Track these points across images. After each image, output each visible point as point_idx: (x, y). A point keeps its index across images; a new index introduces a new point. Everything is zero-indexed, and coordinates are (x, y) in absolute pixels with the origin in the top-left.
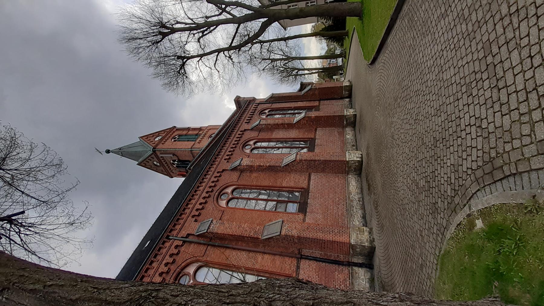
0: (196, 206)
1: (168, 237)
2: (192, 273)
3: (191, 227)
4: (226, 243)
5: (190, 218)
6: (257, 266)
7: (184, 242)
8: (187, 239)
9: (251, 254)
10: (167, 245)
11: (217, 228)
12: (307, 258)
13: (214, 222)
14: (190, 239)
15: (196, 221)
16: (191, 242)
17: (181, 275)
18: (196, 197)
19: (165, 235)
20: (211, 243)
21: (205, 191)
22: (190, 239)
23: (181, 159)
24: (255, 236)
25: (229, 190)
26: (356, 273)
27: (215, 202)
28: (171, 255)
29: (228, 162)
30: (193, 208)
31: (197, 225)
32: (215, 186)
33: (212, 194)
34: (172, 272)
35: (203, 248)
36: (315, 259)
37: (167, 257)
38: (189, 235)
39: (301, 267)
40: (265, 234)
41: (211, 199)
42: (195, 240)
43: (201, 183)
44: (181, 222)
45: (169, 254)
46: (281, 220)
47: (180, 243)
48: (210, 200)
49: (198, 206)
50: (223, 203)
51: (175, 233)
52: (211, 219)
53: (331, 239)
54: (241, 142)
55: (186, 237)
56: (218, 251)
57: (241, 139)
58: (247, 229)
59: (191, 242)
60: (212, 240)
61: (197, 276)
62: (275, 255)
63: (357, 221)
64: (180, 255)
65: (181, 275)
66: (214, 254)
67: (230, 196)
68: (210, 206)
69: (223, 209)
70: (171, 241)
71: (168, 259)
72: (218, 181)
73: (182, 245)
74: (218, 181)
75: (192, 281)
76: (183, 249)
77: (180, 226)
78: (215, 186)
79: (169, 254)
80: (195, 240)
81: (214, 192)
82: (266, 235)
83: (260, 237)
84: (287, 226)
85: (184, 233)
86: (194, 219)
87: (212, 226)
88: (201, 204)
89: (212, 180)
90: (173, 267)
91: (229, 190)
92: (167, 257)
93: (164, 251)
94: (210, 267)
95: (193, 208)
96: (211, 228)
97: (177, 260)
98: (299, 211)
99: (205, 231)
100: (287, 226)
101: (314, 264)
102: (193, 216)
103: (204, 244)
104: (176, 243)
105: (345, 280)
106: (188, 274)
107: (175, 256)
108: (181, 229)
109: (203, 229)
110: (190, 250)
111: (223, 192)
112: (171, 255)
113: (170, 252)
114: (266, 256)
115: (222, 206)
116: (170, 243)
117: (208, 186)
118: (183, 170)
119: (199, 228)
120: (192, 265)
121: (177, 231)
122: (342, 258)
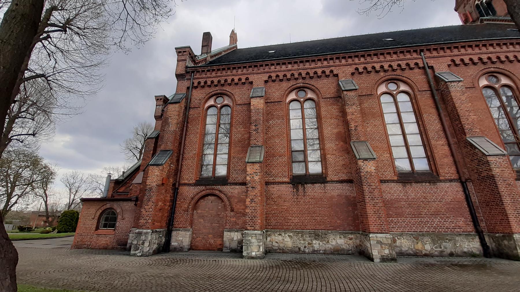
0: (466, 56)
1: (422, 51)
2: (400, 89)
3: (441, 66)
4: (441, 106)
5: (450, 58)
6: (433, 142)
7: (424, 68)
8: (428, 70)
9: (442, 132)
10: (415, 55)
11: (456, 91)
12: (465, 189)
13: (461, 84)
14: (429, 71)
15: (449, 66)
16: (426, 74)
17: (395, 81)
18: (477, 50)
19: (422, 48)
20: (435, 92)
21: (490, 55)
22: (429, 71)
23: (493, 3)
24: (466, 131)
25: (310, 95)
26: (473, 239)
27: (481, 73)
28: (408, 65)
29: (449, 66)
30: (381, 62)
31: (445, 69)
32: (502, 62)
33: (490, 65)
34: (395, 73)
35: (426, 87)
36: (468, 198)
37: (405, 62)
38: (432, 68)
39: (452, 183)
40: (356, 144)
41: (483, 67)
42: (431, 76)
43: (498, 45)
44: (442, 53)
45: (408, 61)
46: (375, 156)
47: (421, 65)
48: (481, 67)
49: (466, 60)
50: (483, 82)
51: (428, 54)
52: (462, 79)
53: (509, 212)
54: (308, 81)
55: (429, 67)
56: (430, 102)
57: (407, 71)
58: (470, 120)
59: (426, 74)
60: (439, 92)
61: (399, 94)
62: (453, 155)
63: (405, 244)
64: (411, 71)
65: (395, 81)
66: (426, 101)
67: (497, 86)
68: (472, 70)
69: (476, 85)
70: (419, 56)
71: (403, 64)
72: (511, 62)
73: (419, 68)
74: (511, 62)
75: (395, 92)
76: (416, 70)
77: (437, 55)
78: (502, 62)
79: (408, 61)
80: (431, 76)
81: (387, 74)
82: (476, 141)
83: (468, 136)
84: (501, 160)
85: (431, 62)
86: (450, 63)
87: (456, 84)
88: (471, 59)
89: (508, 54)
90: (399, 72)
91: (504, 81)
92: (405, 62)
93: (408, 56)
94: (316, 108)
95: (381, 62)
96: (453, 84)
97: (405, 71)
98: (517, 172)
99: (447, 81)
100: (501, 160)
101: (461, 195)
102: (453, 61)
103: (430, 86)
104: (420, 62)
105: (460, 227)
106: (398, 87)
107: (408, 68)
108: (434, 57)
109: (448, 77)
110: (417, 77)
111: (305, 89)
112: (408, 65)
113: (410, 62)
114: (446, 148)
115: (480, 82)
116: (418, 56)
117: (498, 54)
118: (475, 15)
119: (445, 73)
120: (407, 85)
121: (431, 55)
122: (483, 225)
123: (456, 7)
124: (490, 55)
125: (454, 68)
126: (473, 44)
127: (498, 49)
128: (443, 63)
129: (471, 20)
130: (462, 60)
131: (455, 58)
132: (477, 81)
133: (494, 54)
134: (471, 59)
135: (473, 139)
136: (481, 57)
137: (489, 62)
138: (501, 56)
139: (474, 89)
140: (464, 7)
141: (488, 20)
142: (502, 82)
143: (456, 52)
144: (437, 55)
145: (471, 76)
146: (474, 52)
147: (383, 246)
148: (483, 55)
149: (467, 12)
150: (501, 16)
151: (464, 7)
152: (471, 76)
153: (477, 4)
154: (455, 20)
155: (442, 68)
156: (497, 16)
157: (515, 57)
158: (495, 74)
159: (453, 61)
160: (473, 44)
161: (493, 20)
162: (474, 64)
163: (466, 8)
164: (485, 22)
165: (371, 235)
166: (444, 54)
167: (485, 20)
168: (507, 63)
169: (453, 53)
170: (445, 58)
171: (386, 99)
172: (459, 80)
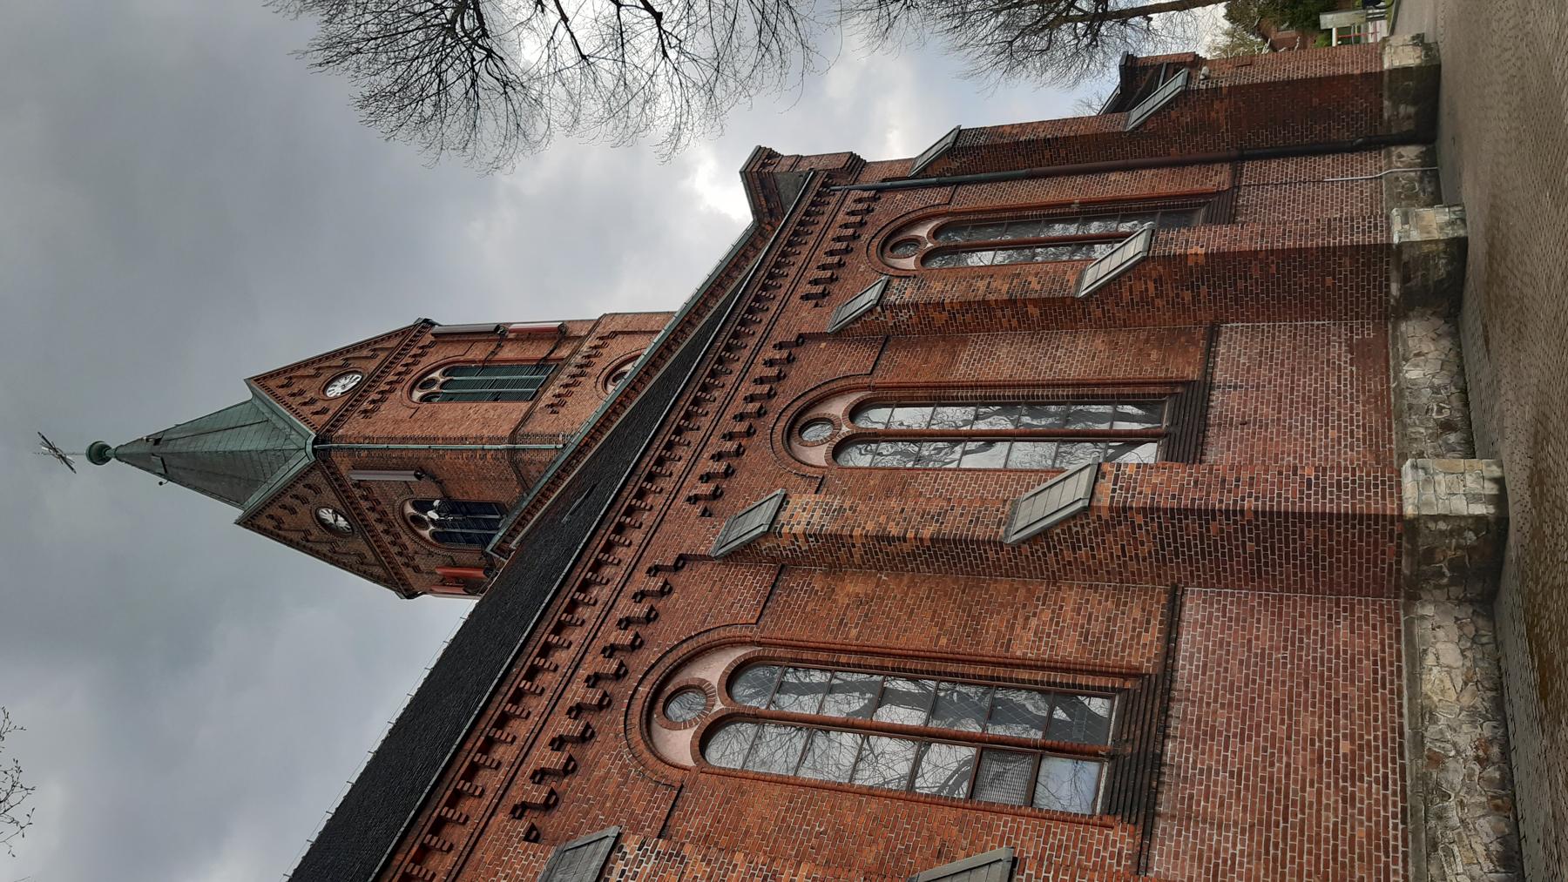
0: (535, 752)
5: (502, 816)
13: (630, 846)
15: (533, 835)
18: (536, 705)
21: (583, 672)
25: (712, 671)
33: (621, 690)
41: (615, 716)
44: (458, 836)
50: (678, 745)
52: (612, 831)
67: (719, 706)
68: (607, 758)
69: (676, 775)
77: (450, 859)
86: (522, 827)
87: (620, 866)
89: (619, 613)
91: (712, 671)
92: (523, 780)
98: (1109, 809)
102: (520, 810)
117: (599, 644)
123: (398, 591)
124: (583, 672)
125: (551, 823)
126: (502, 704)
127: (576, 636)
128: (505, 851)
129: (480, 573)
130: (540, 775)
131: (516, 796)
132: (660, 767)
133: (589, 657)
134: (558, 743)
135: (1020, 524)
136: (569, 704)
137: (610, 687)
138: (612, 639)
139: (687, 793)
140: (417, 569)
141: (511, 535)
142: (715, 683)
143: (490, 781)
144: (450, 859)
145: (626, 776)
146: (534, 718)
147: (1495, 750)
148: (568, 695)
149: (439, 572)
150: (520, 502)
151: (417, 569)
152: (626, 776)
153: (433, 535)
154: (446, 615)
155: (525, 869)
156: (514, 508)
157: (655, 570)
158: (670, 688)
159: (520, 810)
160: (502, 704)
161: (520, 524)
162: (586, 737)
163: (422, 567)
164: (513, 546)
165: (1396, 240)
166: (469, 829)
167: (504, 540)
168: (645, 632)
169: (489, 794)
170: (490, 835)
171: (728, 751)
172: (608, 843)
